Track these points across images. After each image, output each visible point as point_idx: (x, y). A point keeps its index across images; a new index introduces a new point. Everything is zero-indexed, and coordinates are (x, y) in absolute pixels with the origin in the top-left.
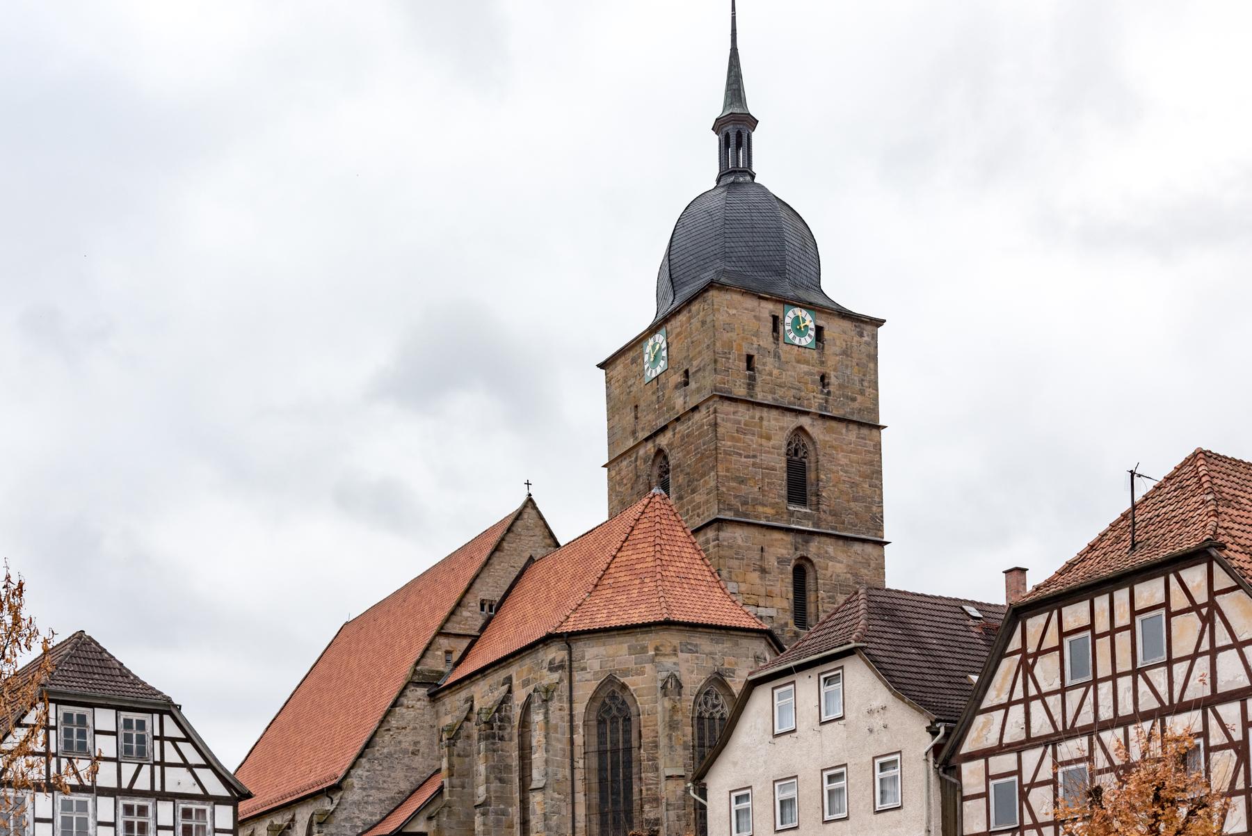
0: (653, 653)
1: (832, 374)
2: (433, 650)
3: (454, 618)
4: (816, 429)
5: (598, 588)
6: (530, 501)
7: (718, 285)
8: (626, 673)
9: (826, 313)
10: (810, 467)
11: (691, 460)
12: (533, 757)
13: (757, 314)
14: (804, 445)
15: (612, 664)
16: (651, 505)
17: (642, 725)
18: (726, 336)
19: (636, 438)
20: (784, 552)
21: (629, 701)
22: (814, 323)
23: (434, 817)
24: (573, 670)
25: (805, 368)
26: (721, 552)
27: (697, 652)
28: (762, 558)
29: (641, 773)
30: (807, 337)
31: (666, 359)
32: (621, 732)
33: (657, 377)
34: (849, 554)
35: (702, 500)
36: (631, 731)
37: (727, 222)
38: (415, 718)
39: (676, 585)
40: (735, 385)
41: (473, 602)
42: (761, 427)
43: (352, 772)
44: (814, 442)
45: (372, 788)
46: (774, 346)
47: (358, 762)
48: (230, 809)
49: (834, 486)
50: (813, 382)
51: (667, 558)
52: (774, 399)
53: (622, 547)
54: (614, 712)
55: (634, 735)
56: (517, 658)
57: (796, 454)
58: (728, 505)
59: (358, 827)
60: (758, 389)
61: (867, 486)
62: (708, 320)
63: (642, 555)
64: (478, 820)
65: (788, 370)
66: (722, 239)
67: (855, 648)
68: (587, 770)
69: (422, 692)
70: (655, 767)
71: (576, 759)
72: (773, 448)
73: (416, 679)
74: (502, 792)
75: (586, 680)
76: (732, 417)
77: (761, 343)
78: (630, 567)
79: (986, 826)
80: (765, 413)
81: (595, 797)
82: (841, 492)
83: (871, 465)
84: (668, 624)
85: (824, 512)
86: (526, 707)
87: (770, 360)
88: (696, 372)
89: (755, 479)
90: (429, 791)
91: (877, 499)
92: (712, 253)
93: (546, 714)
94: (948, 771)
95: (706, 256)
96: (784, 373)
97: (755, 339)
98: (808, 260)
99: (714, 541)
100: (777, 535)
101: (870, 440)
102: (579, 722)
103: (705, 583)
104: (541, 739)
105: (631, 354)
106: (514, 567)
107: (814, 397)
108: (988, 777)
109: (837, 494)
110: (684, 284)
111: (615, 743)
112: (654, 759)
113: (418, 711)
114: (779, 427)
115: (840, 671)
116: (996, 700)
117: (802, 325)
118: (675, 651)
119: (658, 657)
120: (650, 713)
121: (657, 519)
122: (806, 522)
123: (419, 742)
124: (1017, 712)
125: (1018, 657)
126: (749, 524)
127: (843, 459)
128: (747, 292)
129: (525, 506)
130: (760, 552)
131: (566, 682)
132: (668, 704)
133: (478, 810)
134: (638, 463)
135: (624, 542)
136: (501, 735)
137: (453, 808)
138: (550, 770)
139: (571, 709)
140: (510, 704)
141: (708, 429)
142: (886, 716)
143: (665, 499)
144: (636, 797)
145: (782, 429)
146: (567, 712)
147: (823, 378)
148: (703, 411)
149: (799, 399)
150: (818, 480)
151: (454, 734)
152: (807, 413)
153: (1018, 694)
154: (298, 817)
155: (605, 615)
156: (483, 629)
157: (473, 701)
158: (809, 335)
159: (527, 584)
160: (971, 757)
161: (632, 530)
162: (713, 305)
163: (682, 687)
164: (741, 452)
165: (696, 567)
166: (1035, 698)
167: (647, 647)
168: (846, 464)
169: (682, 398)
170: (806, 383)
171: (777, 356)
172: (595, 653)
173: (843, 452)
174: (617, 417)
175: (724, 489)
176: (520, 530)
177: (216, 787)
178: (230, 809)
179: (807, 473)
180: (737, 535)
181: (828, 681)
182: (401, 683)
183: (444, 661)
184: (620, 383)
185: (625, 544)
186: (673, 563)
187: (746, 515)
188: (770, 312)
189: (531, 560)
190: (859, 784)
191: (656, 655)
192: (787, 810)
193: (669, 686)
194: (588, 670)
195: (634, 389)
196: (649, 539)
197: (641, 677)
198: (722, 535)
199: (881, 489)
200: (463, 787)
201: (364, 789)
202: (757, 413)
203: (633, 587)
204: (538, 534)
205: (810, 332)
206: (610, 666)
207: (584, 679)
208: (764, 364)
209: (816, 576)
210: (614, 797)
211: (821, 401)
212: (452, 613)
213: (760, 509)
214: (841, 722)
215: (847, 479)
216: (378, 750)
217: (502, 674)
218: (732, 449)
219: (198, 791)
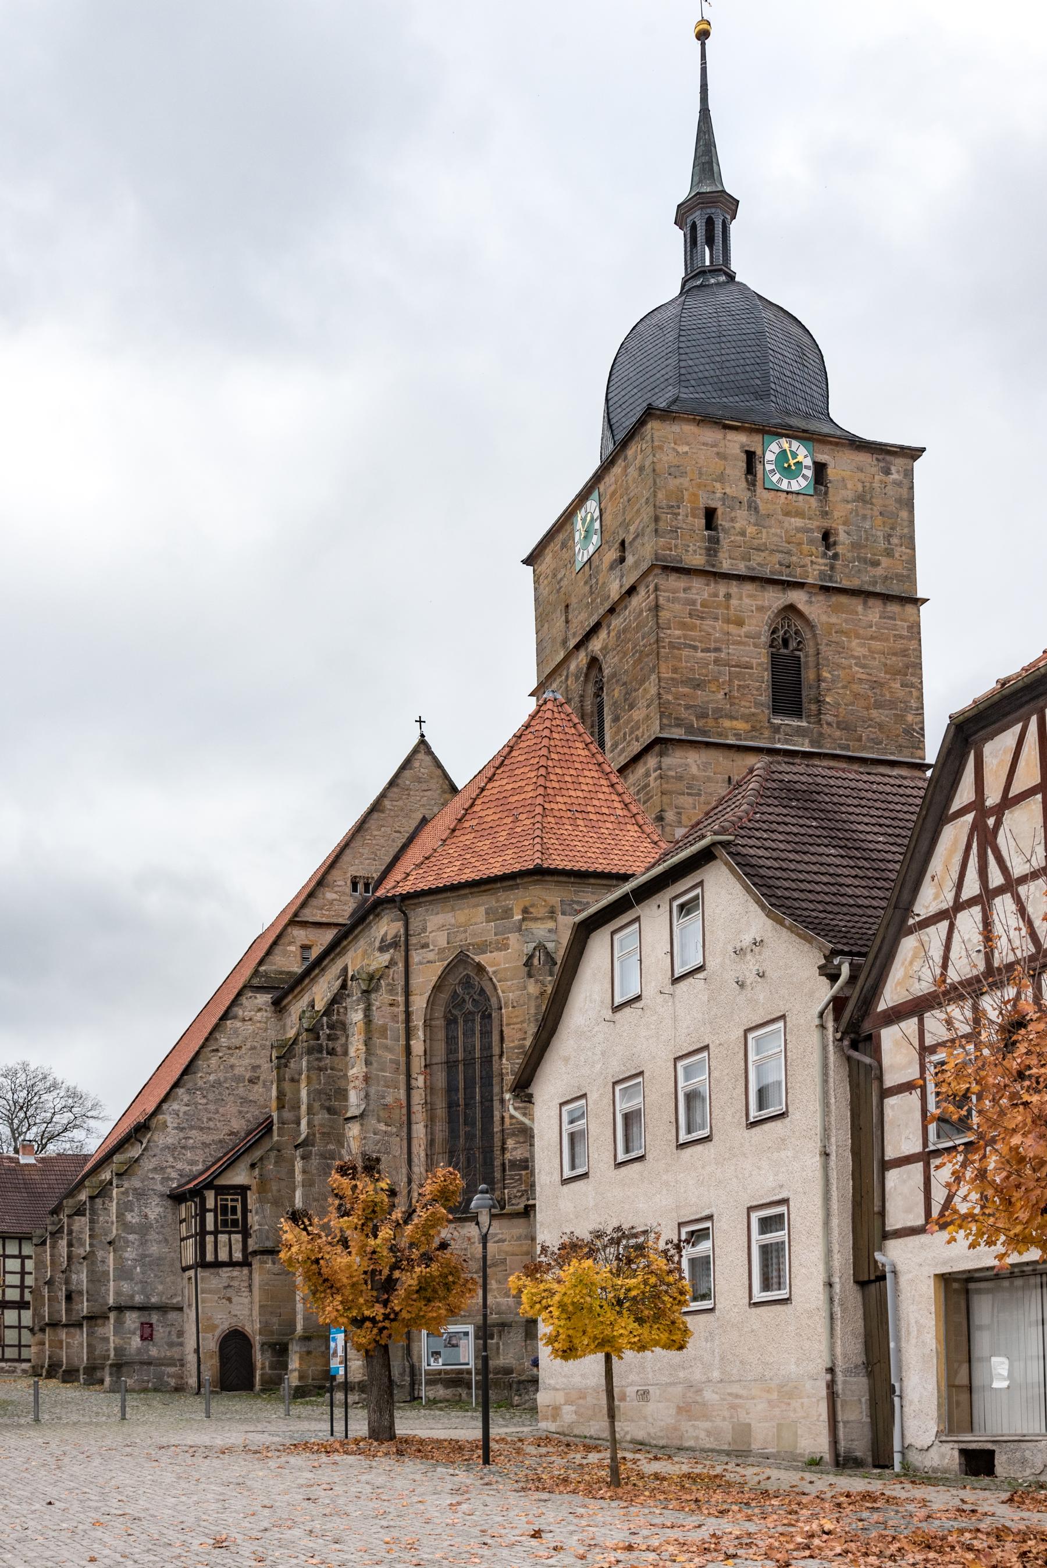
0: (520, 917)
1: (841, 529)
2: (284, 944)
3: (314, 902)
4: (813, 608)
5: (457, 833)
6: (423, 742)
7: (658, 412)
8: (483, 948)
9: (831, 443)
10: (807, 662)
11: (628, 664)
13: (722, 450)
15: (463, 936)
16: (540, 714)
17: (505, 1023)
18: (673, 483)
21: (488, 990)
22: (812, 459)
25: (797, 522)
26: (665, 786)
30: (800, 479)
31: (599, 532)
32: (478, 1034)
35: (641, 717)
37: (682, 333)
38: (255, 1034)
39: (565, 821)
40: (687, 551)
41: (341, 880)
42: (728, 608)
43: (165, 1106)
45: (192, 1128)
46: (749, 494)
47: (173, 1094)
49: (844, 687)
52: (748, 568)
53: (494, 775)
54: (469, 1006)
55: (496, 1037)
56: (350, 939)
57: (785, 643)
58: (676, 719)
59: (172, 1179)
60: (723, 555)
62: (647, 463)
63: (519, 784)
65: (770, 527)
66: (676, 357)
67: (714, 844)
68: (428, 1091)
69: (264, 999)
71: (414, 1076)
72: (746, 637)
73: (256, 982)
74: (331, 1127)
75: (428, 962)
76: (682, 595)
77: (728, 491)
78: (502, 802)
79: (921, 1141)
80: (734, 588)
81: (441, 1129)
82: (856, 695)
83: (905, 656)
84: (540, 873)
85: (829, 724)
88: (634, 539)
91: (914, 704)
92: (662, 379)
94: (861, 1046)
95: (655, 384)
96: (764, 530)
97: (718, 485)
98: (806, 376)
99: (655, 771)
101: (902, 620)
102: (418, 1021)
103: (612, 818)
105: (561, 537)
107: (812, 562)
108: (925, 1050)
109: (849, 698)
111: (469, 1050)
113: (258, 1025)
116: (934, 904)
117: (792, 462)
118: (553, 912)
119: (525, 923)
121: (546, 732)
122: (800, 739)
123: (259, 1067)
124: (969, 922)
125: (969, 818)
126: (708, 745)
127: (859, 649)
128: (706, 419)
129: (415, 751)
131: (401, 965)
134: (569, 682)
135: (498, 768)
138: (372, 1091)
143: (561, 705)
144: (497, 1128)
145: (761, 609)
146: (402, 1008)
147: (826, 536)
148: (642, 591)
149: (789, 567)
150: (819, 679)
152: (800, 585)
153: (972, 887)
158: (804, 476)
160: (895, 1015)
161: (511, 752)
162: (653, 441)
164: (697, 644)
165: (601, 796)
166: (1000, 891)
167: (511, 909)
169: (618, 581)
170: (800, 544)
171: (753, 507)
172: (441, 922)
174: (546, 625)
175: (670, 697)
176: (408, 782)
179: (803, 673)
180: (693, 762)
181: (685, 909)
183: (299, 958)
184: (549, 579)
185: (499, 771)
186: (564, 792)
187: (704, 733)
188: (742, 446)
190: (726, 1078)
191: (524, 919)
192: (635, 1129)
193: (536, 962)
194: (431, 947)
195: (564, 583)
198: (667, 761)
199: (920, 690)
201: (182, 1129)
202: (722, 589)
203: (503, 828)
204: (434, 787)
205: (805, 471)
206: (460, 940)
207: (425, 961)
208: (732, 520)
210: (467, 1129)
213: (727, 723)
214: (701, 975)
215: (864, 677)
218: (682, 641)
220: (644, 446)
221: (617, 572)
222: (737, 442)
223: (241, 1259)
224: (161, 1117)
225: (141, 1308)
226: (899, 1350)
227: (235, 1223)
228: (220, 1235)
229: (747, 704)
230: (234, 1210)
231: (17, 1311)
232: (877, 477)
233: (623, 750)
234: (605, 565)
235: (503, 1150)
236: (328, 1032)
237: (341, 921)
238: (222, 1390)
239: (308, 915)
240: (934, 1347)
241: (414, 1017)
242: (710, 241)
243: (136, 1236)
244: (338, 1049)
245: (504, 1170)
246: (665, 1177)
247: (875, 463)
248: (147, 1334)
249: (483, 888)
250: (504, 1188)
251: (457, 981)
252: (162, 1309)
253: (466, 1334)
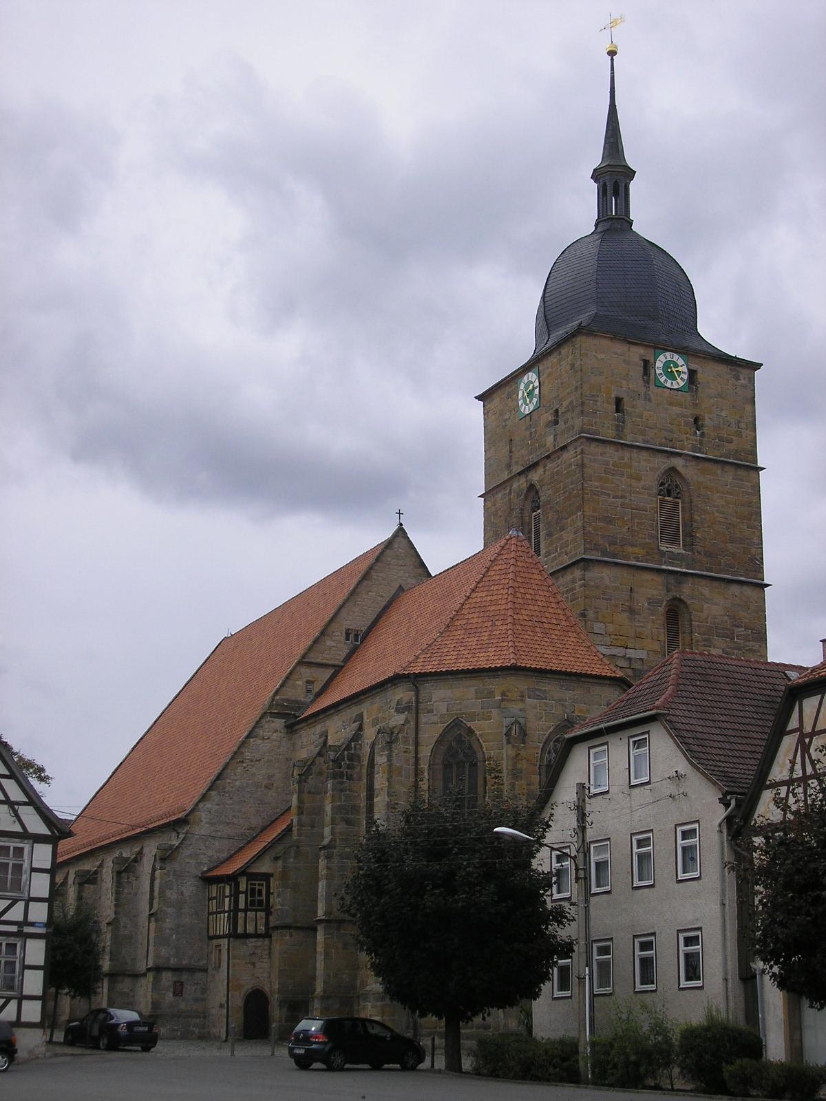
1: (707, 416)
8: (473, 717)
9: (700, 357)
12: (375, 800)
14: (677, 486)
15: (458, 707)
19: (511, 471)
20: (655, 593)
21: (475, 746)
23: (280, 857)
24: (419, 711)
25: (677, 410)
28: (631, 599)
31: (538, 396)
34: (726, 596)
36: (477, 777)
40: (603, 427)
42: (630, 467)
44: (688, 483)
46: (644, 389)
48: (48, 848)
49: (708, 527)
50: (686, 424)
51: (521, 601)
54: (461, 756)
56: (367, 695)
64: (322, 863)
69: (279, 723)
72: (643, 489)
75: (433, 723)
76: (600, 458)
80: (635, 454)
84: (515, 670)
86: (373, 746)
89: (624, 518)
90: (280, 828)
93: (390, 757)
97: (624, 383)
100: (647, 576)
102: (424, 765)
105: (507, 389)
106: (382, 596)
107: (687, 438)
110: (559, 325)
113: (274, 743)
114: (650, 469)
115: (647, 736)
123: (273, 776)
129: (395, 536)
130: (629, 593)
132: (512, 752)
136: (349, 773)
137: (301, 848)
139: (416, 752)
140: (360, 742)
142: (686, 784)
145: (652, 469)
146: (412, 754)
147: (696, 420)
148: (571, 451)
151: (307, 770)
154: (146, 850)
155: (454, 657)
156: (348, 658)
157: (327, 736)
159: (395, 616)
161: (487, 571)
162: (580, 350)
163: (526, 735)
164: (609, 492)
165: (551, 610)
167: (494, 692)
168: (722, 505)
171: (647, 398)
173: (718, 492)
175: (591, 529)
176: (389, 559)
177: (36, 825)
178: (48, 848)
180: (605, 576)
181: (638, 744)
182: (259, 712)
183: (305, 691)
185: (480, 585)
186: (526, 606)
188: (641, 356)
189: (401, 589)
191: (502, 700)
193: (513, 732)
194: (435, 713)
195: (509, 423)
196: (503, 582)
198: (589, 575)
200: (313, 826)
202: (627, 454)
207: (430, 722)
209: (690, 618)
211: (694, 442)
212: (316, 641)
213: (630, 549)
214: (647, 787)
215: (722, 520)
216: (229, 783)
217: (354, 711)
219: (18, 828)
222: (637, 353)
223: (263, 932)
225: (174, 970)
226: (764, 1019)
227: (260, 903)
228: (249, 913)
229: (643, 536)
230: (260, 892)
231: (42, 963)
232: (730, 381)
233: (555, 558)
234: (542, 423)
236: (348, 762)
237: (337, 662)
238: (245, 1038)
239: (313, 658)
240: (782, 1018)
241: (421, 762)
242: (616, 193)
243: (174, 910)
246: (624, 906)
247: (729, 371)
248: (178, 990)
249: (476, 675)
251: (453, 738)
252: (191, 970)
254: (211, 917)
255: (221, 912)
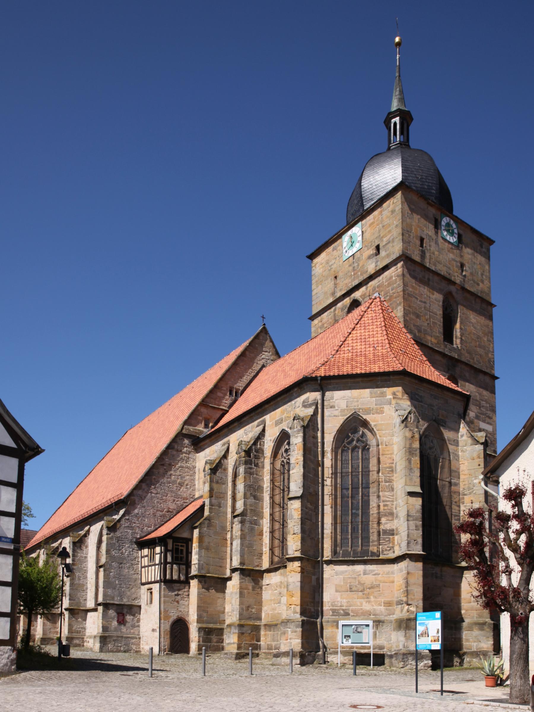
1: (467, 265)
17: (381, 453)
27: (422, 402)
29: (379, 492)
33: (353, 255)
52: (435, 269)
55: (373, 462)
61: (486, 339)
70: (392, 487)
71: (325, 479)
75: (335, 416)
87: (433, 244)
88: (386, 244)
104: (299, 458)
112: (390, 481)
120: (387, 444)
129: (261, 331)
133: (236, 519)
141: (396, 279)
144: (373, 511)
194: (336, 408)
197: (380, 415)
207: (333, 415)
220: (395, 201)
221: (374, 259)
224: (132, 497)
231: (9, 579)
235: (379, 523)
244: (260, 464)
245: (379, 535)
250: (379, 545)
253: (368, 626)
254: (143, 569)
255: (153, 565)
